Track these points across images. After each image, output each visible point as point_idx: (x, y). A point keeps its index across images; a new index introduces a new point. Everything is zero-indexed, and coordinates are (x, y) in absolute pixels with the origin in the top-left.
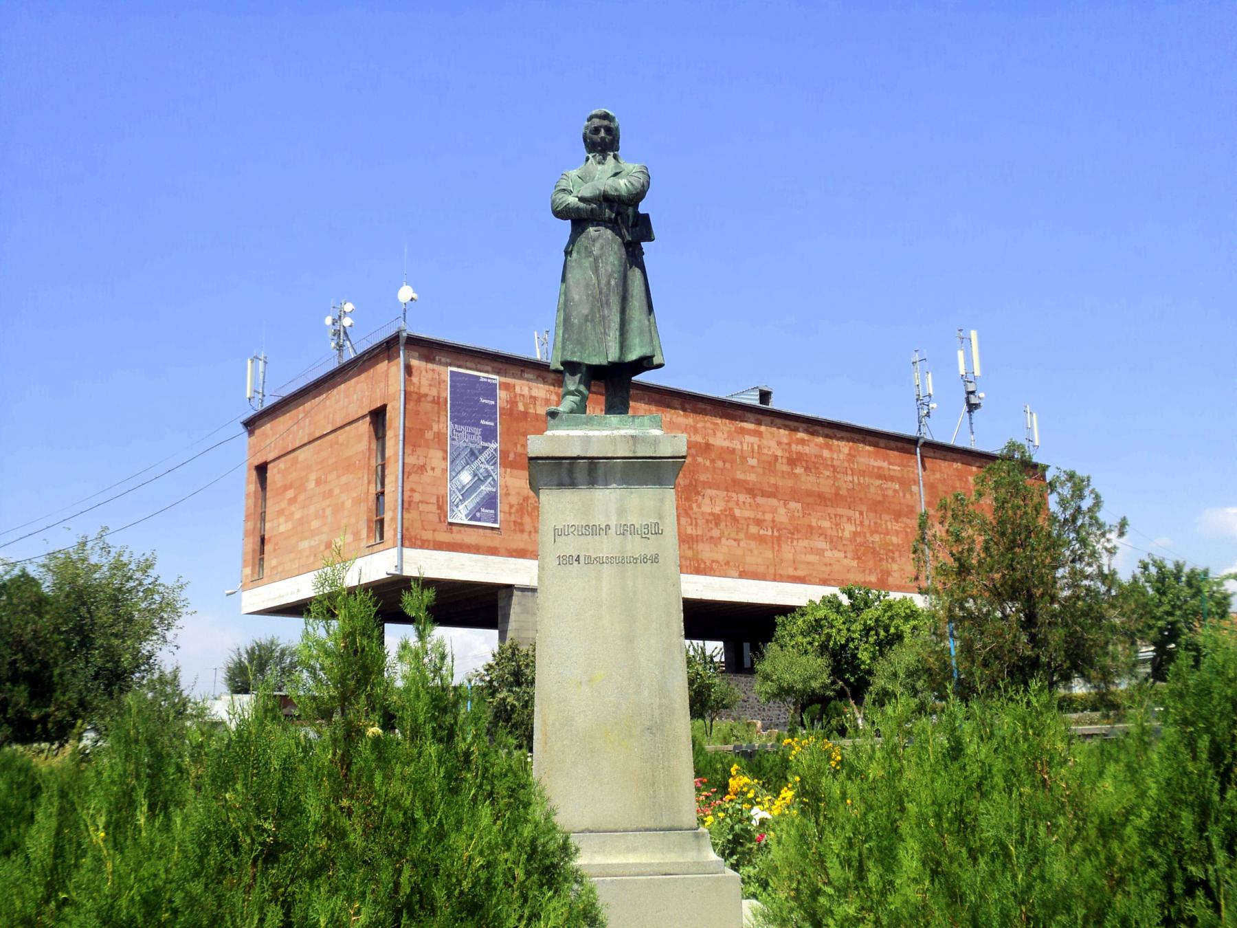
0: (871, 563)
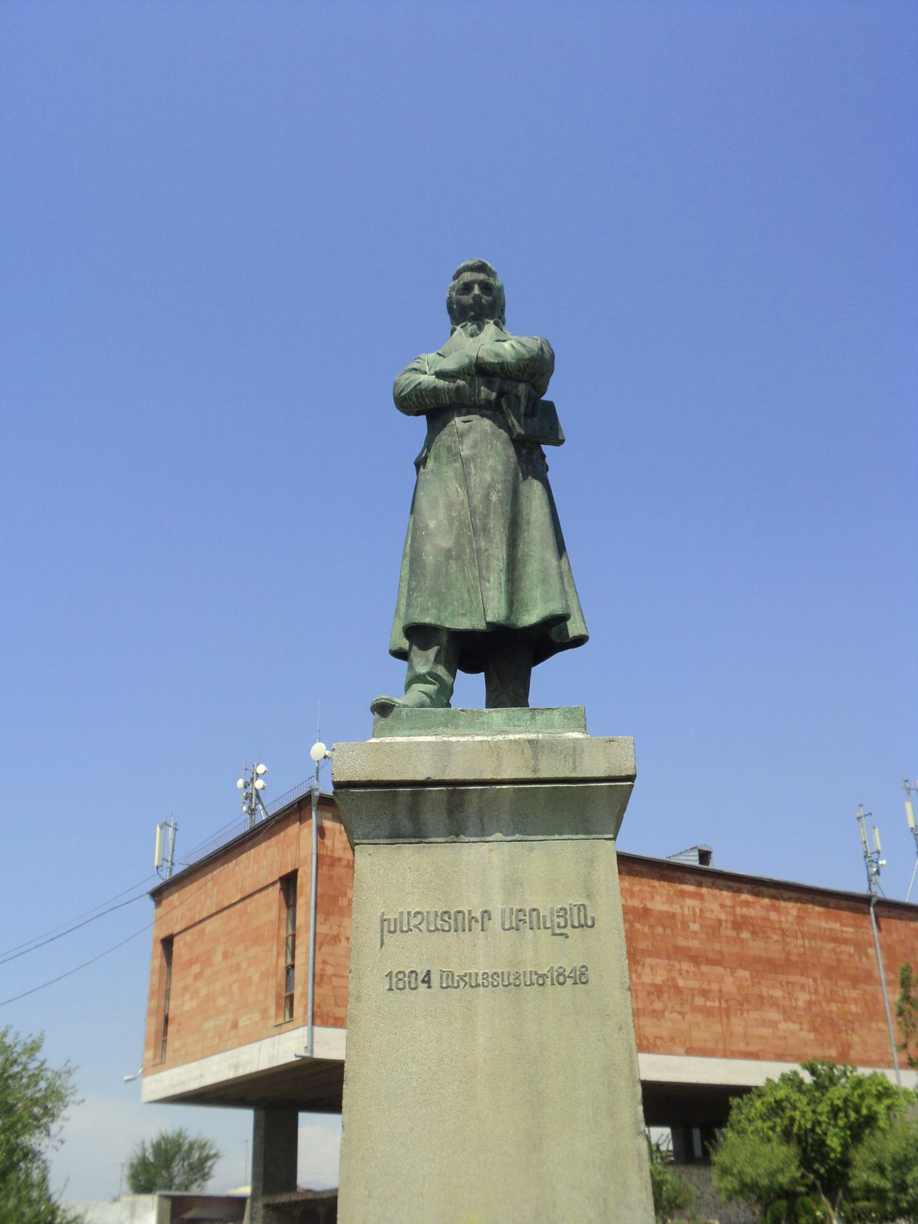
0: (829, 1036)
